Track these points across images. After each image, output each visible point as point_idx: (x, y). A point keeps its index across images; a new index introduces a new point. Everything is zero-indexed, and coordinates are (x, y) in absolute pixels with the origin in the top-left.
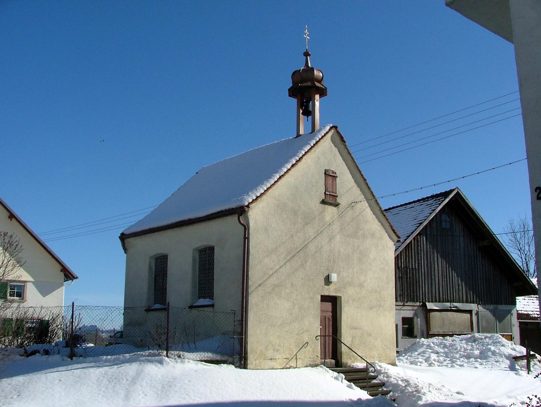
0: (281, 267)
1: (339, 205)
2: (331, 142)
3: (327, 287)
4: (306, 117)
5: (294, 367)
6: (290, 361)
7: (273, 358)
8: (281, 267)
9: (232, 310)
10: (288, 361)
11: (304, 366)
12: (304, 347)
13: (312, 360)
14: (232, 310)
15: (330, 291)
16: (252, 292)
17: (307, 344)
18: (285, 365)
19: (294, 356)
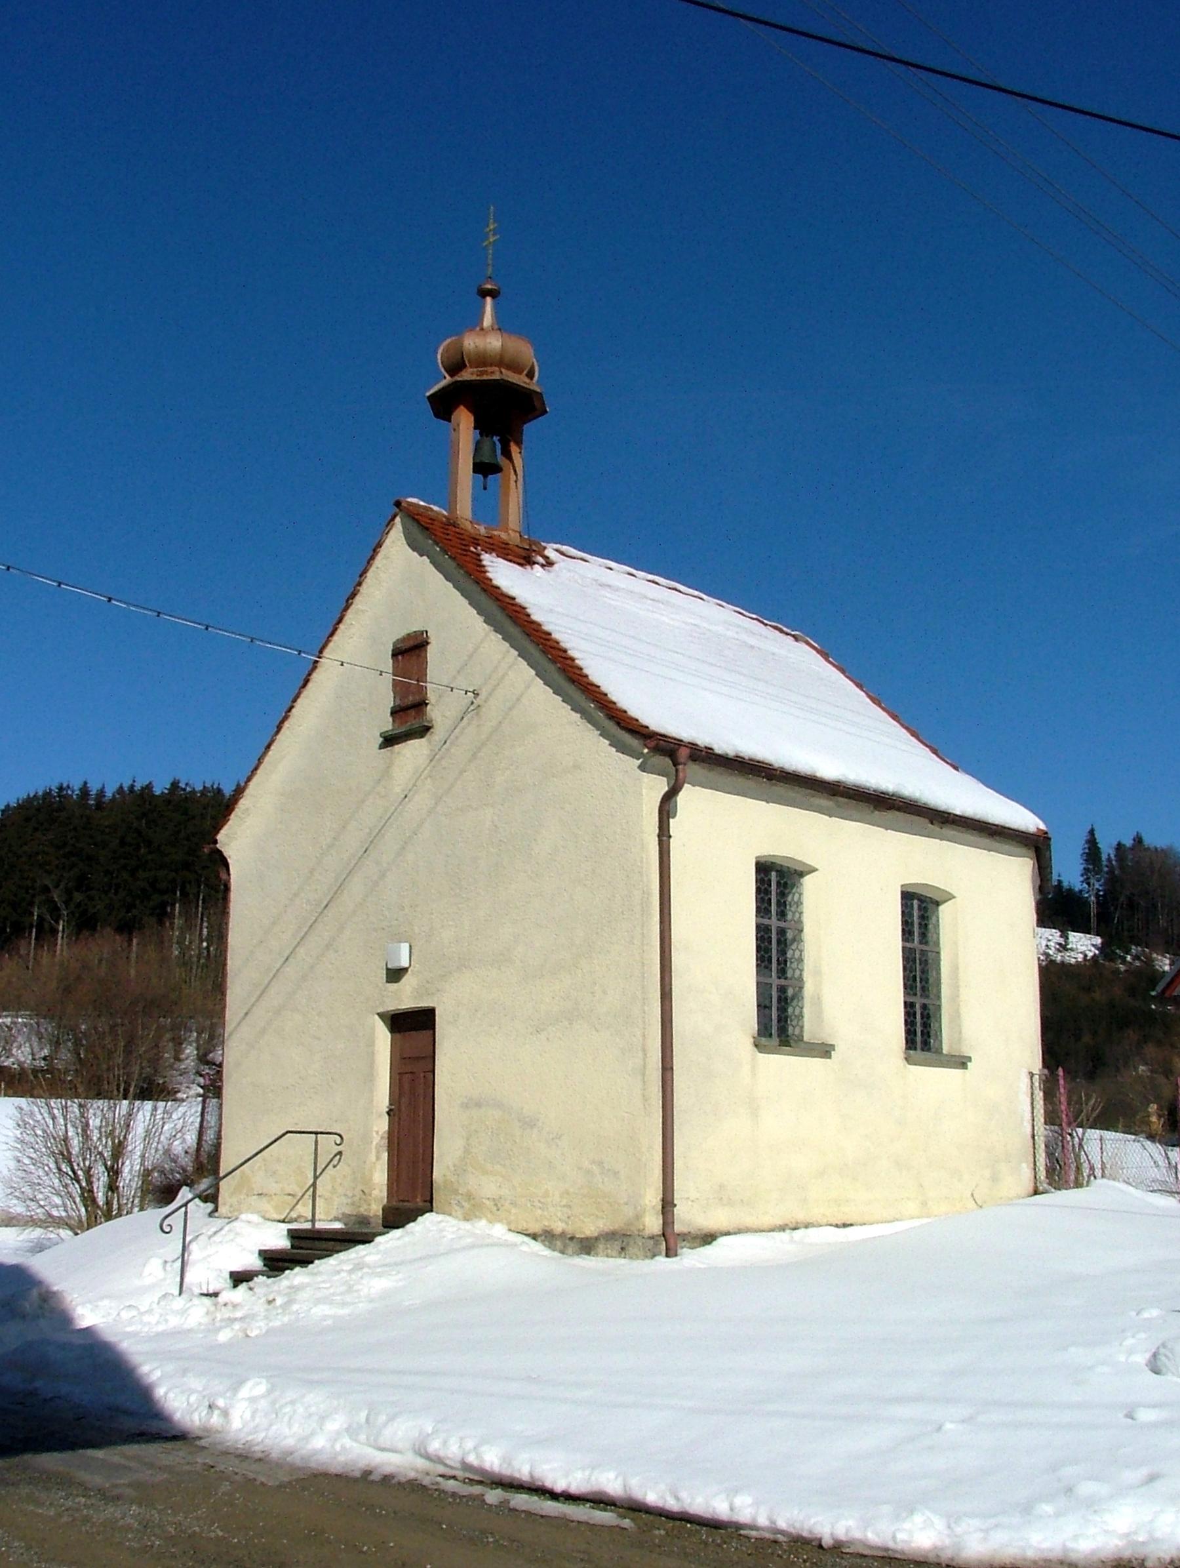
0: (287, 959)
1: (424, 646)
2: (947, 890)
3: (393, 987)
4: (480, 476)
5: (306, 1217)
6: (299, 1201)
7: (265, 1191)
8: (287, 959)
9: (217, 1252)
10: (295, 1201)
11: (332, 1217)
12: (331, 1166)
13: (349, 1201)
14: (217, 1252)
15: (405, 997)
16: (230, 1035)
17: (338, 1157)
18: (289, 1214)
19: (310, 1187)
